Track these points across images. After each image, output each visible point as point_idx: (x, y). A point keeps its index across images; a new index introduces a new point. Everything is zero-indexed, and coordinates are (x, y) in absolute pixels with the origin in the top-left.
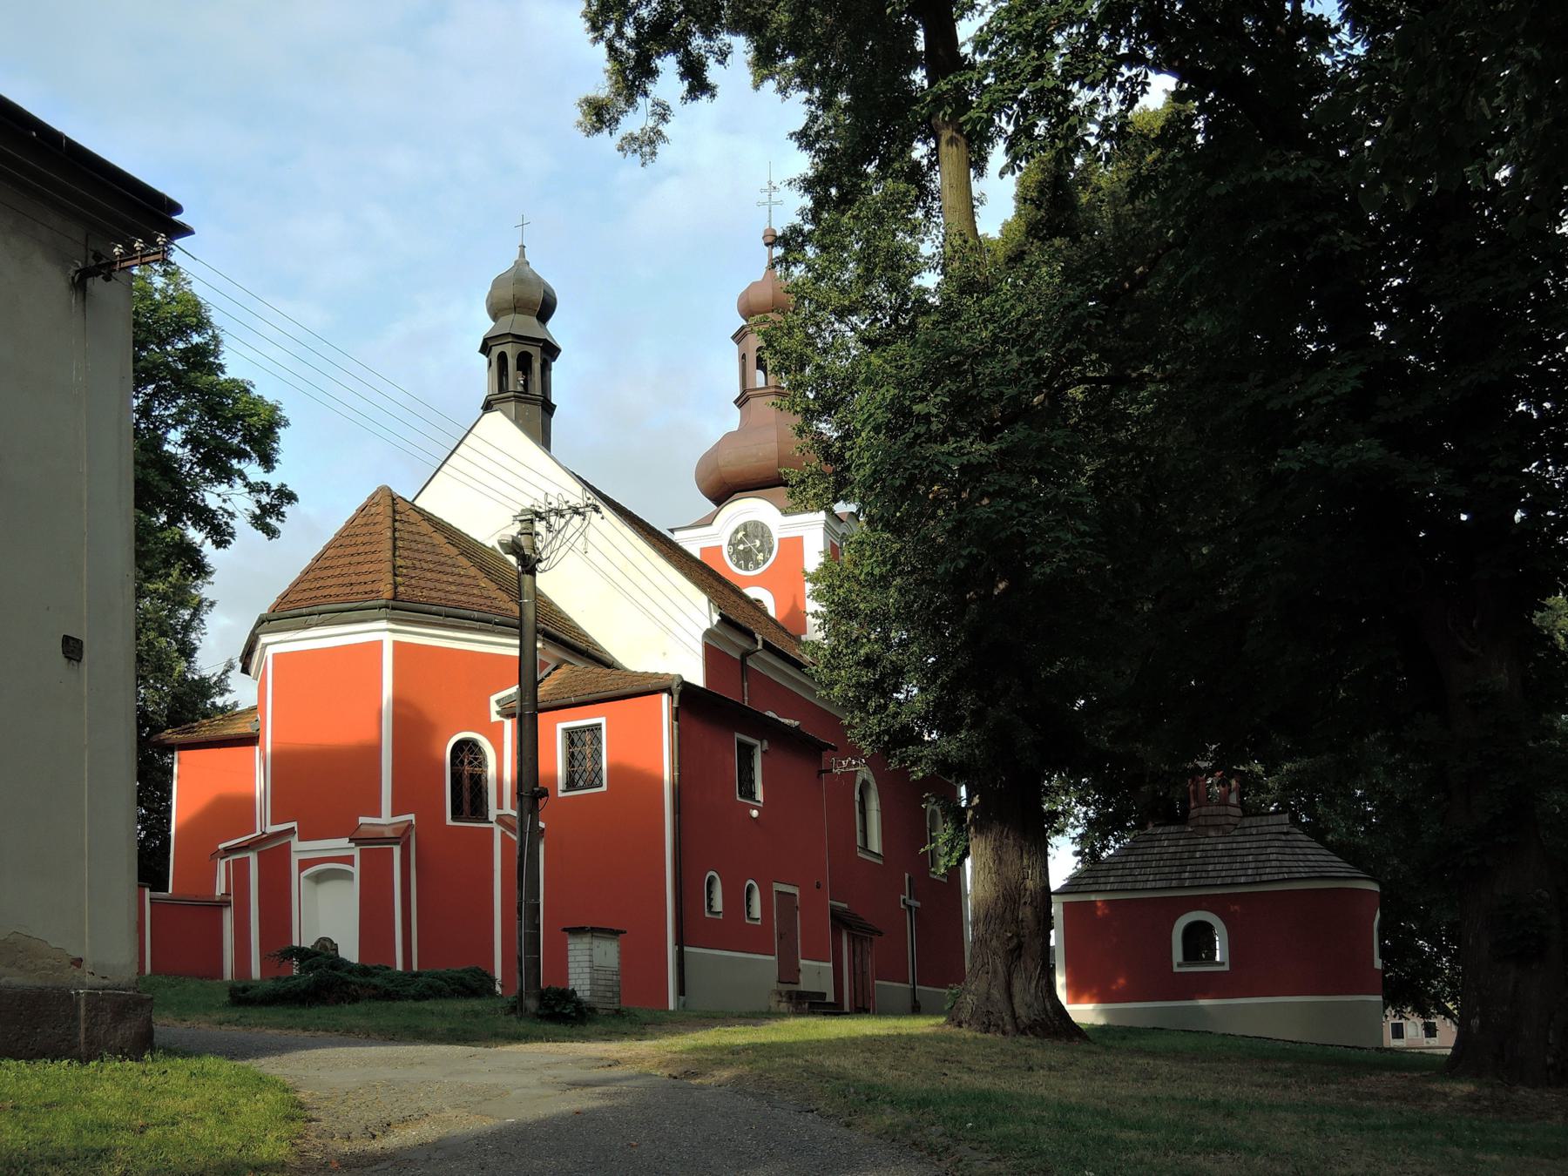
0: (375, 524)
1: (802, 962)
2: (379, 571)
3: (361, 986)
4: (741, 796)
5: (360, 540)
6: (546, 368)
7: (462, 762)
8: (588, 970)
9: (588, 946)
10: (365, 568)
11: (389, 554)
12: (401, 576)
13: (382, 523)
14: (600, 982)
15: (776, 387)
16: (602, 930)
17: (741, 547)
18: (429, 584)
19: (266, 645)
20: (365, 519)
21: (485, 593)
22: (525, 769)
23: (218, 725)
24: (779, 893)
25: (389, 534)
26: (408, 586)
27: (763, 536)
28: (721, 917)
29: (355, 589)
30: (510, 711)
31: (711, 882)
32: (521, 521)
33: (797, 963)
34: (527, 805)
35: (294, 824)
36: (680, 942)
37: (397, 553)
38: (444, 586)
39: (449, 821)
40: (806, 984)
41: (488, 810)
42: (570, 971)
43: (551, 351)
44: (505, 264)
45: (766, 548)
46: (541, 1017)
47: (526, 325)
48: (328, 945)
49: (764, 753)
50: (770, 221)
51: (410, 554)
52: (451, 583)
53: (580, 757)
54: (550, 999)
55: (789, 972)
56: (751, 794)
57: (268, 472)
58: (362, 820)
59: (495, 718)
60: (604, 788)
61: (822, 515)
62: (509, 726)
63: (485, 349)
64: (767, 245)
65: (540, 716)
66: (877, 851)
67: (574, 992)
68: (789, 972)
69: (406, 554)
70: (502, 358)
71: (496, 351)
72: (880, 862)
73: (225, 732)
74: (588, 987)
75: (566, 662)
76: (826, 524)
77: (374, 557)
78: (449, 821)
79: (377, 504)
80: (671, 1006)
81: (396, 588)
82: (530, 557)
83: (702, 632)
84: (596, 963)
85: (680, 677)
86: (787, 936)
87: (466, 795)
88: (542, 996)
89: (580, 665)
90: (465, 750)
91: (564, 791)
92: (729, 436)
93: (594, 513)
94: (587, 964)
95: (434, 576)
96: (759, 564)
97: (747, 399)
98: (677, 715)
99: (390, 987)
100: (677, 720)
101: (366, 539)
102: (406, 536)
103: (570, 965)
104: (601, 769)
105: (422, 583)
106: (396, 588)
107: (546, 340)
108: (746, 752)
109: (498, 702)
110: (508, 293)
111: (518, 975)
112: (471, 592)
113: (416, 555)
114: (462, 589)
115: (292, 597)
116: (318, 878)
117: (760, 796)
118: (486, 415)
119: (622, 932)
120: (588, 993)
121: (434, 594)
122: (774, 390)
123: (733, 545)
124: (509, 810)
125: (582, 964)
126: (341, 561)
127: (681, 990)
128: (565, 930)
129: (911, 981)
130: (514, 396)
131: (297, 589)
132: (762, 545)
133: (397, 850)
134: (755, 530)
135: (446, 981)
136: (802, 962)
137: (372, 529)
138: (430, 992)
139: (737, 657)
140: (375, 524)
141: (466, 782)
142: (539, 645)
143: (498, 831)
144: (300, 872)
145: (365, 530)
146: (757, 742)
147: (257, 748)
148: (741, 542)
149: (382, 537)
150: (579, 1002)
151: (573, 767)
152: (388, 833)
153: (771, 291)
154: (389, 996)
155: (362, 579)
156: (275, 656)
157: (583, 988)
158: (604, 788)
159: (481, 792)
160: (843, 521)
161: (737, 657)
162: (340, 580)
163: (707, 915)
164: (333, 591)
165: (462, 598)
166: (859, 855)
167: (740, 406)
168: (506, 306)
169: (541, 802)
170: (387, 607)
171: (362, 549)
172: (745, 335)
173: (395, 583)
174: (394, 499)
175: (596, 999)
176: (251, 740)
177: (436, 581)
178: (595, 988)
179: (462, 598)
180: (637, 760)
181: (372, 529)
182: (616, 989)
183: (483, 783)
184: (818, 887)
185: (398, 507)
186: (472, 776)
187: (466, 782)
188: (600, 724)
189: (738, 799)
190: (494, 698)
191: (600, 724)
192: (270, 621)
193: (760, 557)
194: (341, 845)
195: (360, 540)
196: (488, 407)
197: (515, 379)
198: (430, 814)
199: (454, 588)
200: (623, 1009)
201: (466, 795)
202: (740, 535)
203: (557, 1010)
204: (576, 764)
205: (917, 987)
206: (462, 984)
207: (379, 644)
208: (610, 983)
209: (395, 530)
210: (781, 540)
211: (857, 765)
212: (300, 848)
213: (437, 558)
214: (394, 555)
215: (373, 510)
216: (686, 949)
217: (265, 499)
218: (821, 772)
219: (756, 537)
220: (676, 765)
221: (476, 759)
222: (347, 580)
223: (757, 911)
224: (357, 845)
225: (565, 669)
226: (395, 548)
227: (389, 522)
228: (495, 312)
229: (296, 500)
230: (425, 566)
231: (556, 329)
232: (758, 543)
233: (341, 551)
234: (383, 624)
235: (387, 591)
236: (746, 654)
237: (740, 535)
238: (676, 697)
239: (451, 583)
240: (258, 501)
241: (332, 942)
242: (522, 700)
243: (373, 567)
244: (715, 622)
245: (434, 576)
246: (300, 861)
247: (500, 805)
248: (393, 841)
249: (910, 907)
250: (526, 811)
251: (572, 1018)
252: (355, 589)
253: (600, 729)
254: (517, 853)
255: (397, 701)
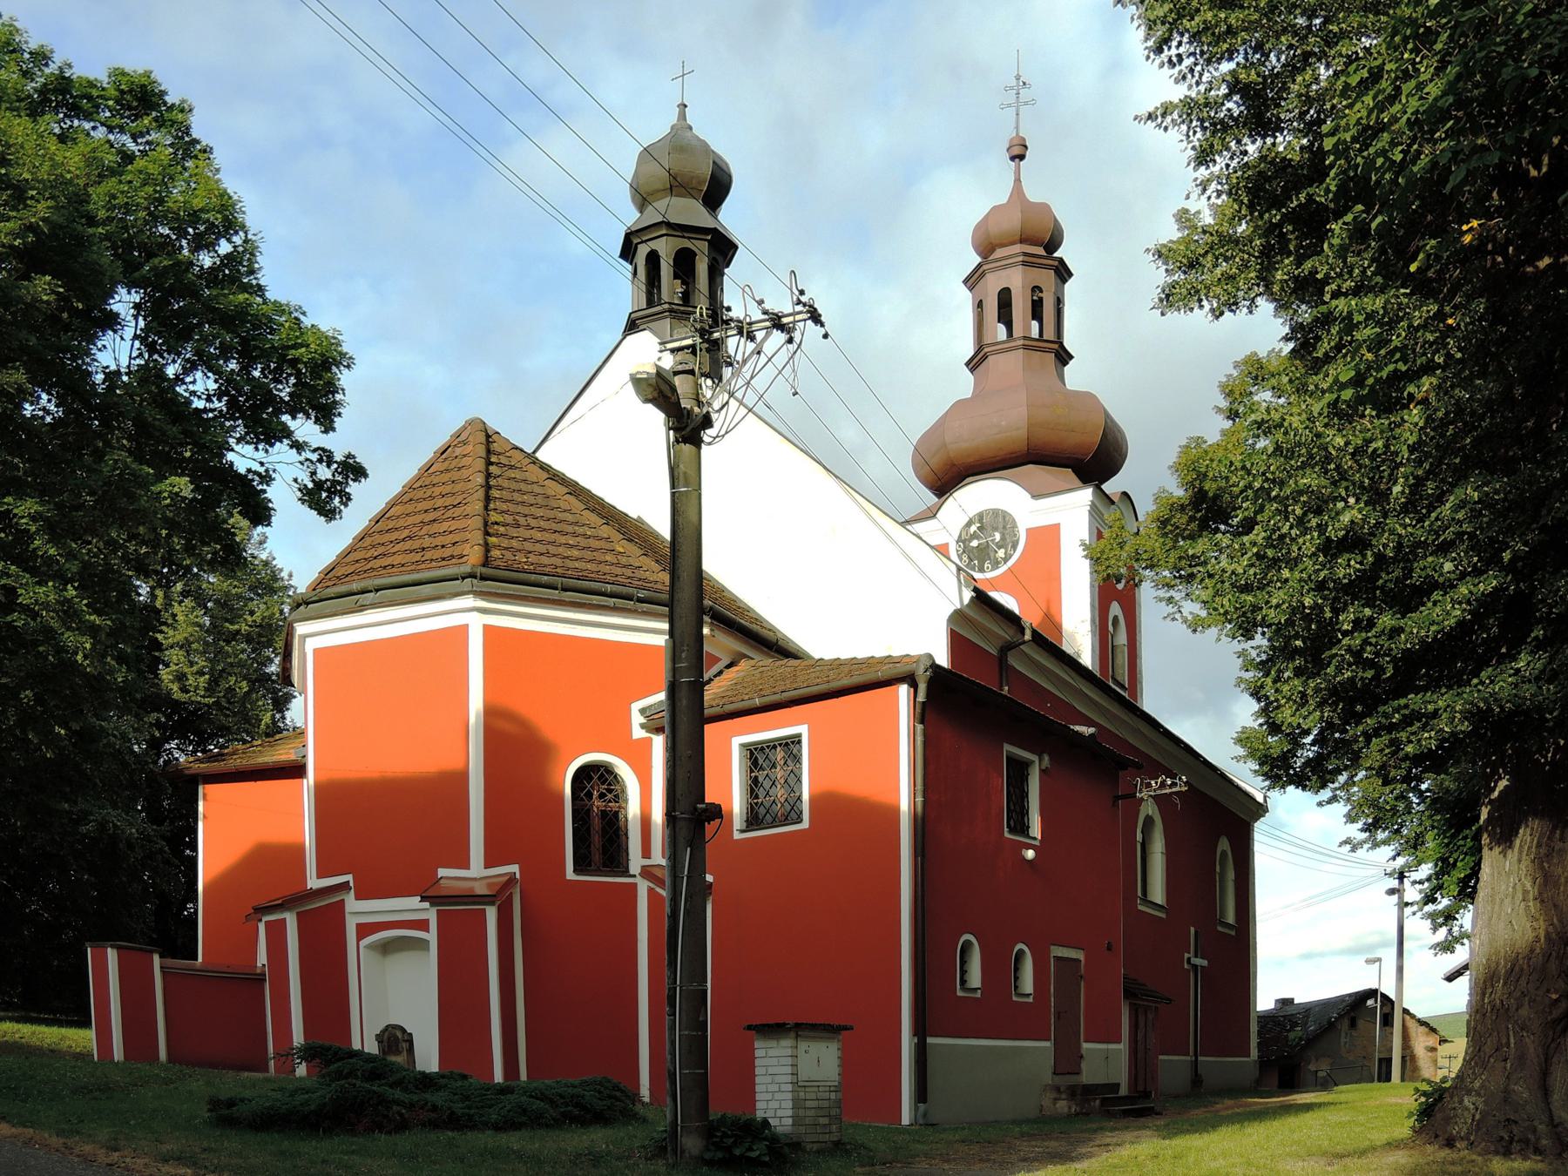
0: (460, 469)
1: (1085, 1046)
2: (464, 529)
3: (411, 1106)
4: (1011, 831)
5: (437, 490)
6: (716, 274)
7: (590, 795)
8: (790, 1087)
9: (789, 1052)
10: (445, 526)
11: (479, 506)
12: (497, 535)
13: (470, 466)
14: (809, 1104)
15: (1025, 338)
16: (814, 1027)
17: (975, 543)
18: (540, 548)
19: (304, 637)
20: (447, 463)
21: (624, 560)
22: (681, 774)
23: (254, 752)
24: (1058, 959)
25: (480, 479)
26: (506, 549)
27: (1004, 527)
28: (978, 994)
29: (428, 555)
30: (658, 724)
31: (967, 947)
32: (673, 351)
33: (1079, 1047)
34: (683, 833)
35: (349, 878)
36: (920, 1030)
37: (492, 506)
38: (561, 550)
39: (570, 874)
40: (1090, 1073)
41: (628, 860)
42: (758, 1088)
43: (723, 249)
44: (657, 128)
45: (1009, 542)
46: (710, 1163)
47: (691, 212)
48: (399, 1034)
49: (1043, 772)
50: (1017, 128)
51: (512, 507)
52: (572, 546)
53: (767, 784)
54: (725, 1135)
55: (1068, 1060)
56: (1021, 827)
57: (326, 432)
58: (442, 872)
59: (638, 733)
60: (805, 824)
61: (1086, 495)
62: (659, 743)
63: (628, 252)
64: (1013, 158)
65: (708, 728)
66: (1160, 903)
67: (765, 1122)
68: (1068, 1060)
69: (504, 507)
70: (653, 259)
71: (643, 251)
72: (1163, 915)
73: (260, 760)
74: (790, 1113)
75: (745, 656)
76: (1093, 506)
77: (457, 512)
78: (570, 874)
79: (465, 443)
80: (906, 1119)
81: (487, 551)
82: (690, 412)
83: (950, 610)
84: (803, 1076)
85: (930, 656)
86: (1066, 1016)
87: (596, 840)
88: (710, 1131)
89: (767, 662)
90: (595, 778)
91: (742, 831)
92: (960, 405)
93: (809, 322)
94: (789, 1078)
95: (547, 536)
96: (998, 563)
97: (985, 357)
98: (924, 714)
99: (459, 1107)
100: (922, 722)
101: (447, 489)
102: (506, 484)
103: (758, 1080)
104: (799, 798)
105: (528, 546)
106: (487, 551)
107: (715, 230)
108: (1019, 772)
109: (642, 711)
110: (659, 175)
111: (669, 1100)
112: (602, 558)
113: (520, 509)
114: (588, 554)
115: (339, 572)
116: (386, 948)
117: (1036, 829)
118: (628, 337)
119: (846, 1028)
120: (790, 1121)
121: (545, 560)
122: (1021, 342)
123: (964, 542)
124: (659, 858)
125: (784, 1087)
126: (411, 520)
127: (921, 1094)
128: (749, 1028)
129: (1191, 1053)
130: (670, 311)
131: (346, 560)
132: (1003, 538)
133: (491, 914)
134: (995, 521)
135: (552, 1102)
136: (1085, 1046)
137: (455, 475)
138: (524, 1119)
139: (994, 652)
140: (460, 469)
141: (596, 823)
142: (706, 631)
143: (643, 887)
144: (359, 940)
145: (446, 478)
146: (1034, 758)
147: (305, 781)
148: (974, 536)
149: (470, 485)
150: (775, 1139)
151: (757, 797)
152: (481, 889)
153: (1020, 215)
154: (455, 1122)
155: (439, 541)
156: (318, 652)
157: (780, 1113)
158: (805, 824)
159: (618, 836)
160: (1113, 503)
161: (994, 652)
162: (408, 545)
163: (960, 993)
164: (397, 560)
165: (589, 566)
166: (1140, 907)
167: (972, 370)
168: (659, 186)
169: (710, 828)
170: (472, 576)
171: (439, 502)
172: (983, 275)
173: (486, 544)
174: (489, 437)
175: (802, 1130)
176: (296, 770)
177: (549, 543)
178: (801, 1113)
179: (589, 566)
180: (857, 784)
181: (455, 475)
182: (833, 1112)
183: (622, 823)
184: (1109, 949)
185: (495, 447)
186: (604, 814)
187: (596, 823)
188: (799, 735)
189: (1007, 835)
190: (636, 707)
191: (799, 735)
192: (307, 604)
193: (1001, 553)
194: (410, 906)
195: (437, 490)
196: (632, 326)
197: (670, 288)
198: (541, 863)
199: (575, 553)
200: (845, 1140)
201: (596, 840)
202: (973, 528)
203: (737, 1152)
204: (761, 793)
205: (1200, 1058)
206: (577, 1105)
207: (463, 630)
208: (826, 1104)
209: (488, 475)
210: (1029, 531)
211: (1174, 784)
212: (357, 910)
213: (551, 514)
214: (486, 508)
215: (458, 451)
216: (930, 1040)
217: (324, 473)
218: (1118, 798)
219: (996, 529)
220: (919, 787)
221: (610, 791)
222: (416, 544)
223: (1028, 984)
224: (432, 904)
225: (744, 665)
226: (488, 499)
227: (480, 464)
228: (642, 199)
229: (365, 475)
230: (533, 523)
231: (730, 217)
232: (998, 536)
233: (410, 508)
234: (469, 601)
235: (474, 555)
236: (1007, 648)
237: (973, 528)
238: (922, 687)
239: (572, 546)
240: (313, 473)
241: (403, 1030)
242: (675, 658)
243: (454, 525)
244: (966, 600)
245: (547, 536)
246: (359, 926)
247: (646, 853)
248: (487, 899)
249: (1195, 967)
250: (681, 841)
251: (765, 1164)
252: (428, 555)
253: (799, 742)
254: (668, 910)
255: (490, 712)
